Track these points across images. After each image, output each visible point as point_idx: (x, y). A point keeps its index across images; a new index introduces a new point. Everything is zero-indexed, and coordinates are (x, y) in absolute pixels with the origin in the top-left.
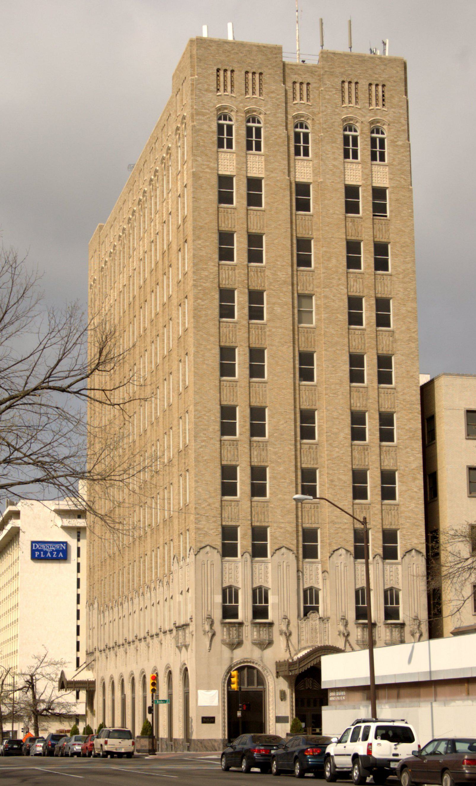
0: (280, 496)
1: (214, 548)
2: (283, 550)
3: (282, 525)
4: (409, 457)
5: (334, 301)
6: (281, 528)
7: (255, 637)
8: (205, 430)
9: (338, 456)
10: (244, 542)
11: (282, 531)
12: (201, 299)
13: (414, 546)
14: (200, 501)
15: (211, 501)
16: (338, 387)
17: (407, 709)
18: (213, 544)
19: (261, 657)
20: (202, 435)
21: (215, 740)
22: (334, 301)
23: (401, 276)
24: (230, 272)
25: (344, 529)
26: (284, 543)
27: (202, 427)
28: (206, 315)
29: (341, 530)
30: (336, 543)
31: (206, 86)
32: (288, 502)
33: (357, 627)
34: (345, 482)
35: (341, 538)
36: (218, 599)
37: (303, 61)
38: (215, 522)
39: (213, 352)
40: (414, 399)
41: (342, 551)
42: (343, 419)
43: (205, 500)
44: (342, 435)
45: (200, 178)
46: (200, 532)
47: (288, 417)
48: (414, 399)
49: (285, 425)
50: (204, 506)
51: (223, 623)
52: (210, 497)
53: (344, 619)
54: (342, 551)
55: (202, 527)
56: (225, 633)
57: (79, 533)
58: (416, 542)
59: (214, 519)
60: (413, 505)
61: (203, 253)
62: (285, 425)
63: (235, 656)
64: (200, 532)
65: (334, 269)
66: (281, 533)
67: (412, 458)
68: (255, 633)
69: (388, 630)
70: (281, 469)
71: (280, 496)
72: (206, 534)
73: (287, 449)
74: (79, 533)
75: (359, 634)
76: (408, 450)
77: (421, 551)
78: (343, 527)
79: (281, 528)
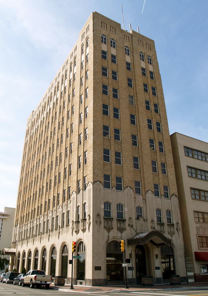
0: (126, 165)
1: (101, 183)
2: (129, 188)
3: (128, 177)
4: (169, 159)
5: (141, 99)
6: (127, 178)
7: (119, 226)
8: (97, 132)
9: (146, 153)
10: (113, 182)
11: (128, 179)
12: (96, 84)
13: (174, 193)
14: (95, 161)
15: (100, 161)
16: (144, 128)
17: (186, 197)
18: (100, 180)
19: (121, 236)
20: (96, 133)
21: (101, 279)
22: (141, 99)
23: (160, 98)
24: (106, 80)
25: (150, 182)
26: (129, 185)
27: (96, 130)
28: (98, 90)
29: (149, 183)
30: (148, 188)
31: (98, 24)
32: (129, 168)
33: (158, 225)
34: (149, 164)
35: (149, 186)
36: (103, 206)
37: (127, 31)
38: (101, 171)
39: (100, 104)
40: (168, 138)
41: (150, 192)
42: (147, 140)
43: (97, 161)
44: (147, 146)
45: (96, 48)
46: (95, 174)
47: (128, 134)
48: (168, 138)
49: (127, 137)
50: (97, 163)
51: (104, 218)
52: (99, 160)
53: (152, 221)
54: (150, 192)
55: (96, 172)
56: (106, 223)
57: (2, 220)
58: (175, 191)
59: (101, 170)
60: (172, 177)
61: (97, 70)
62: (127, 137)
63: (110, 235)
64: (95, 174)
65: (140, 89)
66: (128, 177)
67: (170, 159)
68: (119, 224)
69: (169, 227)
70: (126, 154)
71: (126, 165)
72: (97, 176)
73: (128, 147)
74: (2, 220)
75: (159, 228)
76: (169, 156)
77: (177, 195)
78: (150, 182)
79: (127, 178)
